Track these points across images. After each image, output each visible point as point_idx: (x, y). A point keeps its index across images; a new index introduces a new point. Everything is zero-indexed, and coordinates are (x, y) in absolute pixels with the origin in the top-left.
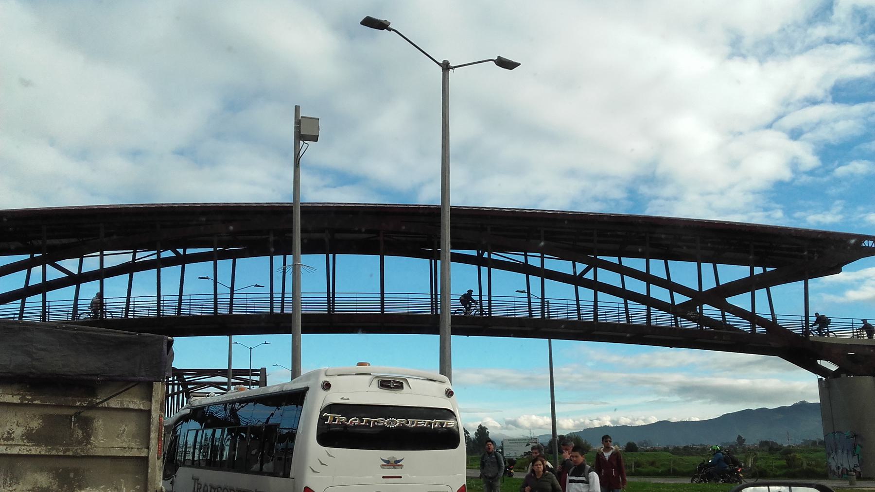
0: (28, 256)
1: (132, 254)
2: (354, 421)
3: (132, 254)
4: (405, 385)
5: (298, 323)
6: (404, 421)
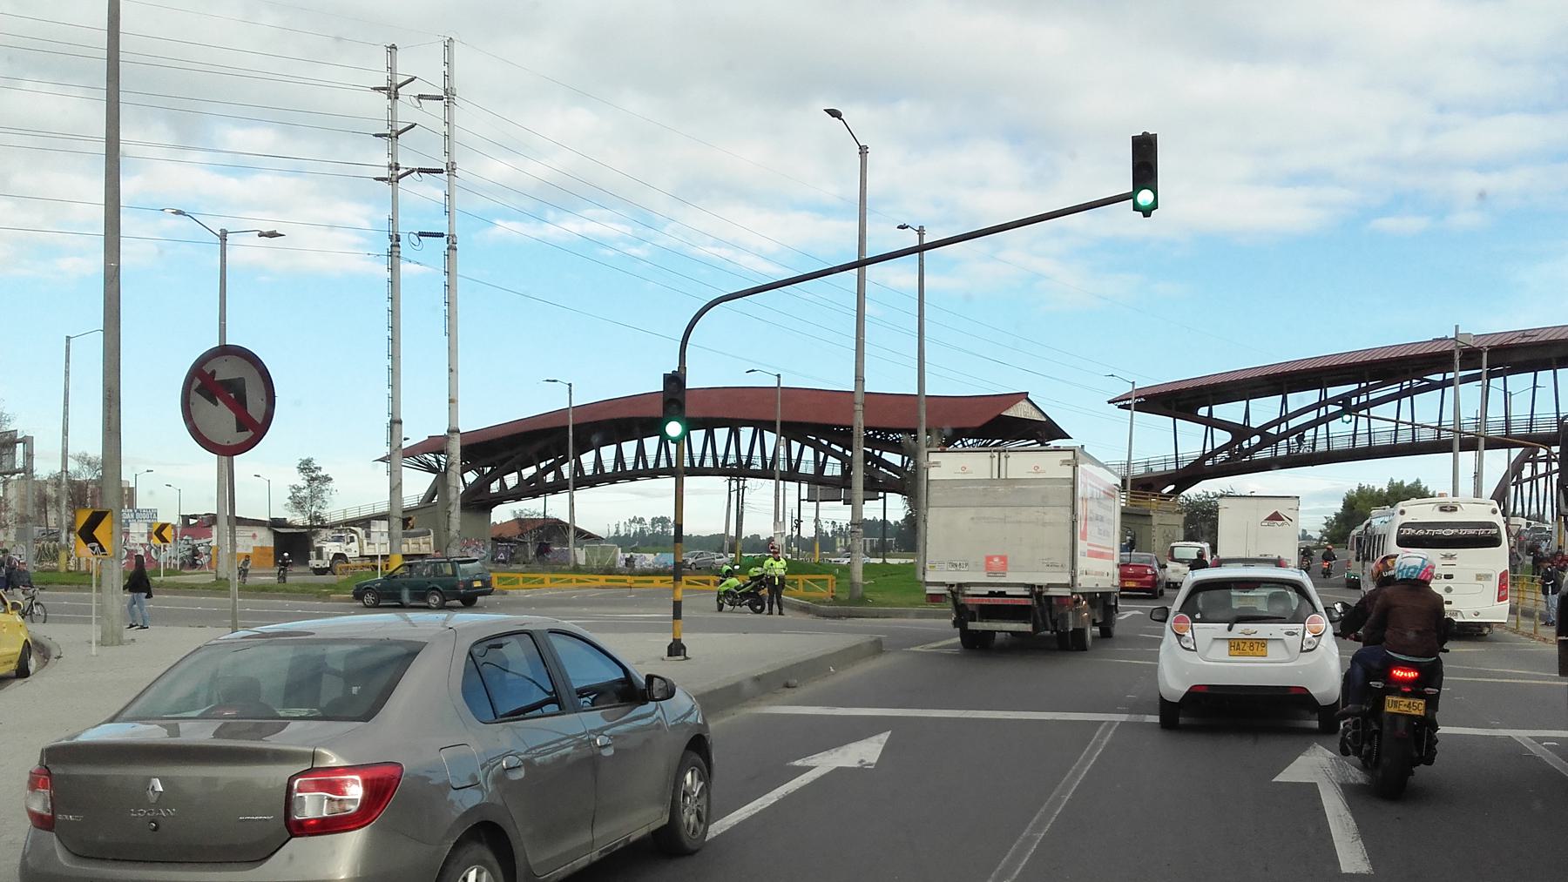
0: (1356, 386)
1: (1214, 429)
2: (1421, 532)
3: (1214, 429)
4: (1459, 508)
5: (1457, 445)
6: (1457, 531)
